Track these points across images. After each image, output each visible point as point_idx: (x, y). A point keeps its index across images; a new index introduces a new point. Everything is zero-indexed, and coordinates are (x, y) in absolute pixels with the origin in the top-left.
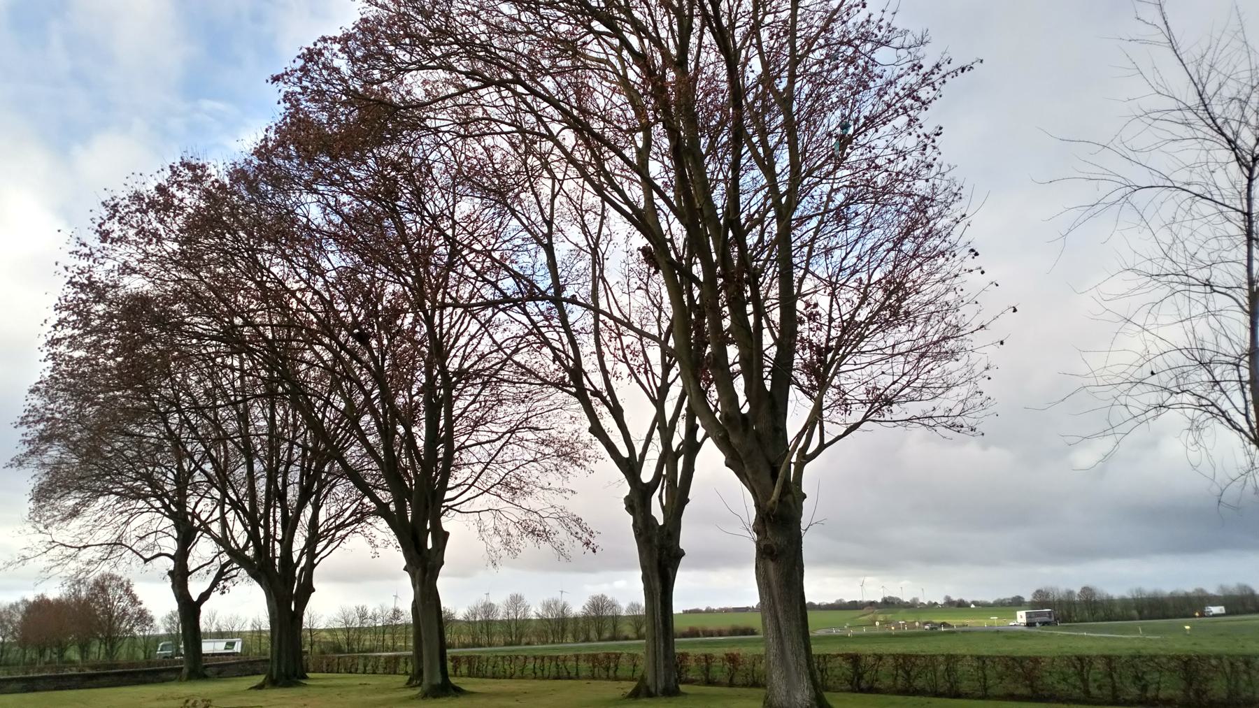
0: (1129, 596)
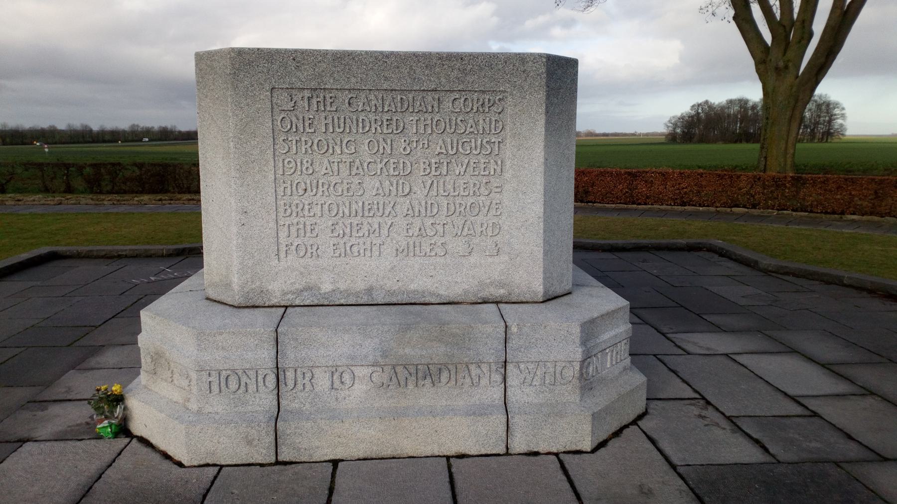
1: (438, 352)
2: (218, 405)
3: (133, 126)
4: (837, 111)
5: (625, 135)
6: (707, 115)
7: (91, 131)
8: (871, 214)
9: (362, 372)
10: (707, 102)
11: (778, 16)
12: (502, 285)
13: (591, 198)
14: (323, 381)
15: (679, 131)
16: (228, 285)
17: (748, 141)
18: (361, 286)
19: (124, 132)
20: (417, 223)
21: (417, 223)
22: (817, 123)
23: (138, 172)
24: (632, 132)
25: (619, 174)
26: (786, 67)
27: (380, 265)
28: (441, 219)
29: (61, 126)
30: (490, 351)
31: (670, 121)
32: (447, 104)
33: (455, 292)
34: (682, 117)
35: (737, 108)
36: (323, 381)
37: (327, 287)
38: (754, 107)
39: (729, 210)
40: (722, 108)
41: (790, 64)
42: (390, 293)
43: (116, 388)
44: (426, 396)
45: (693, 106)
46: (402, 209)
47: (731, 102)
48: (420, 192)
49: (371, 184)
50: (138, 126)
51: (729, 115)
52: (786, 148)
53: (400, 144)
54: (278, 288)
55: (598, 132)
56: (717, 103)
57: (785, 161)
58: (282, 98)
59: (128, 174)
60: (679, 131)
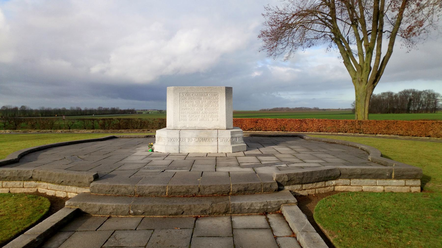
0: (39, 109)
1: (206, 136)
2: (170, 144)
3: (100, 107)
4: (438, 98)
7: (81, 110)
8: (386, 134)
9: (193, 139)
11: (358, 62)
12: (218, 126)
13: (286, 130)
14: (187, 140)
18: (194, 126)
19: (95, 110)
20: (203, 115)
21: (203, 115)
22: (428, 104)
23: (119, 122)
24: (338, 108)
26: (362, 81)
27: (198, 123)
28: (208, 114)
29: (68, 108)
30: (215, 136)
32: (209, 95)
33: (210, 127)
35: (387, 97)
36: (187, 140)
37: (188, 126)
38: (396, 96)
39: (336, 133)
40: (380, 97)
41: (363, 80)
43: (152, 144)
44: (204, 143)
46: (201, 112)
47: (384, 94)
48: (204, 110)
49: (196, 108)
50: (102, 108)
51: (383, 100)
52: (365, 111)
53: (201, 101)
54: (179, 127)
57: (365, 116)
58: (181, 95)
59: (115, 122)
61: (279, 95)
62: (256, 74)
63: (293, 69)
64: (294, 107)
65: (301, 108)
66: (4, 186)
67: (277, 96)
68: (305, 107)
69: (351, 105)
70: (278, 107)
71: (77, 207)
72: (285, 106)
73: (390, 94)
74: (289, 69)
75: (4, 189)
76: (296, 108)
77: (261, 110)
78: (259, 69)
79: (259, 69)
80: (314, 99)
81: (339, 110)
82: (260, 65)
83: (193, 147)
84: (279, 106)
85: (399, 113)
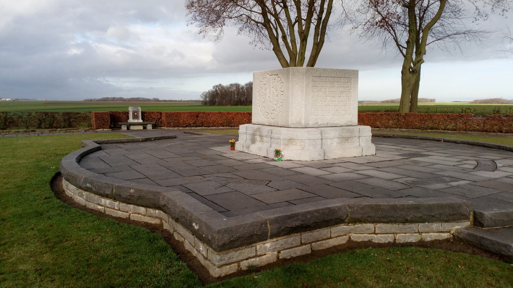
1: (348, 135)
5: (176, 101)
6: (221, 91)
10: (220, 85)
12: (351, 122)
15: (207, 99)
16: (300, 123)
17: (241, 105)
18: (326, 122)
24: (180, 100)
25: (244, 114)
31: (203, 94)
34: (209, 92)
37: (320, 123)
38: (243, 88)
42: (331, 124)
45: (214, 87)
47: (231, 85)
55: (160, 99)
56: (225, 85)
60: (207, 99)
61: (108, 81)
62: (74, 51)
63: (125, 49)
64: (130, 97)
65: (138, 98)
66: (303, 242)
67: (105, 82)
68: (142, 97)
69: (200, 97)
70: (109, 97)
71: (504, 264)
72: (117, 95)
73: (237, 86)
74: (120, 48)
75: (304, 246)
76: (132, 98)
77: (85, 101)
78: (78, 46)
79: (78, 46)
80: (151, 88)
81: (181, 101)
82: (80, 40)
83: (299, 151)
84: (110, 96)
85: (246, 105)
